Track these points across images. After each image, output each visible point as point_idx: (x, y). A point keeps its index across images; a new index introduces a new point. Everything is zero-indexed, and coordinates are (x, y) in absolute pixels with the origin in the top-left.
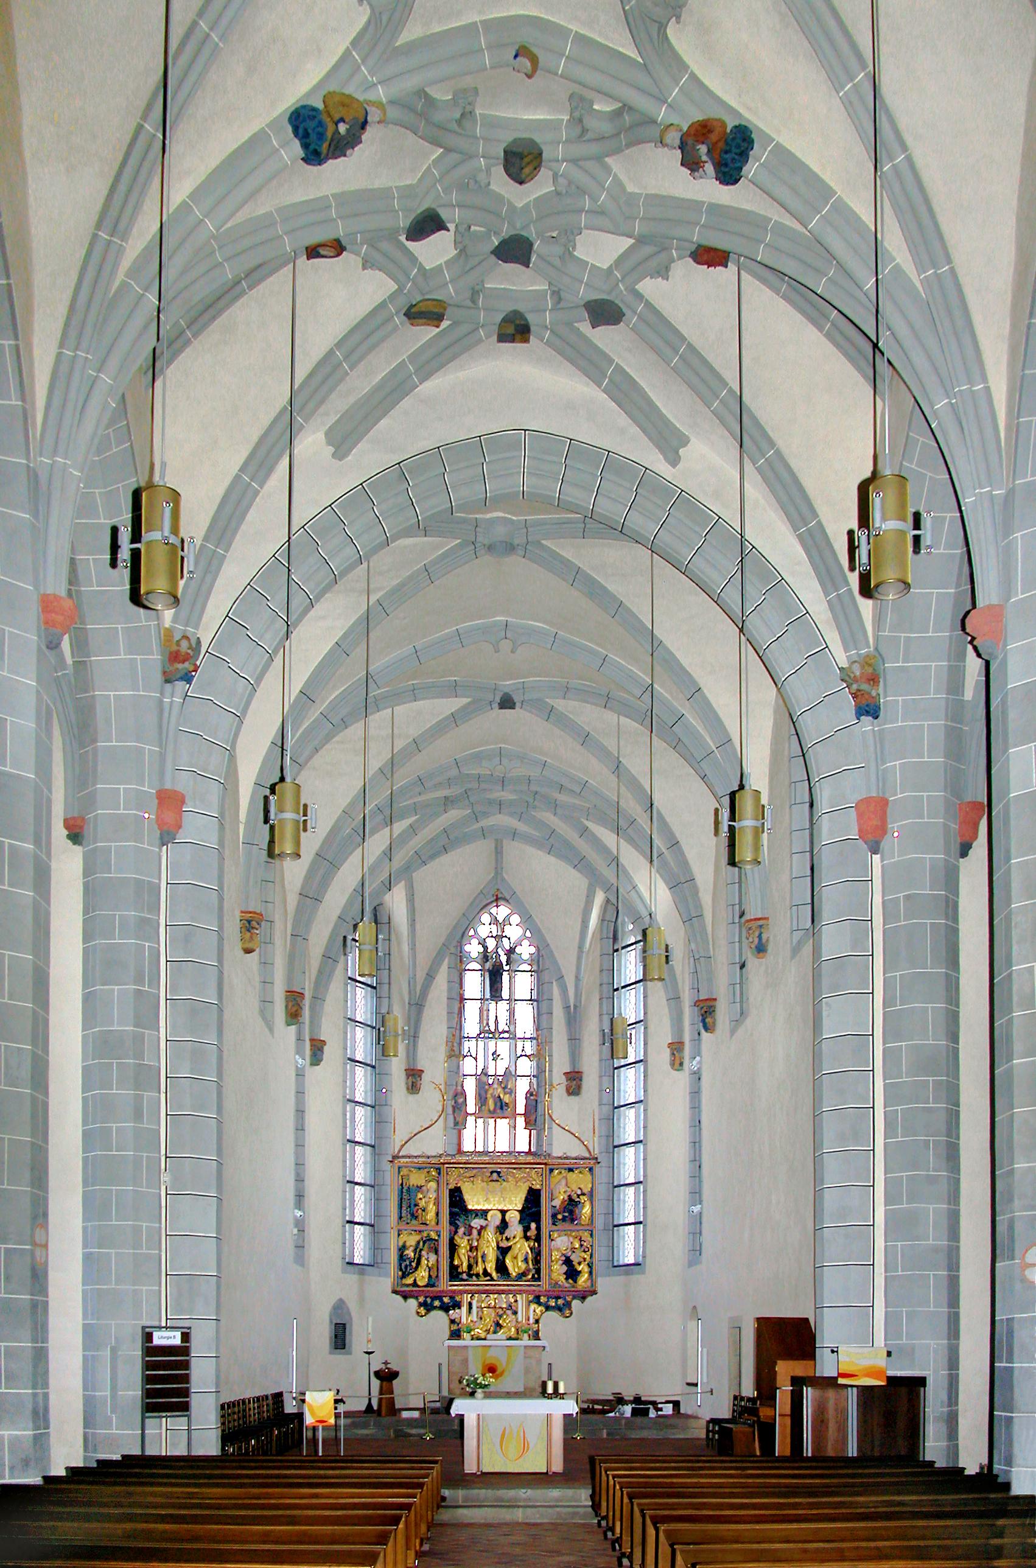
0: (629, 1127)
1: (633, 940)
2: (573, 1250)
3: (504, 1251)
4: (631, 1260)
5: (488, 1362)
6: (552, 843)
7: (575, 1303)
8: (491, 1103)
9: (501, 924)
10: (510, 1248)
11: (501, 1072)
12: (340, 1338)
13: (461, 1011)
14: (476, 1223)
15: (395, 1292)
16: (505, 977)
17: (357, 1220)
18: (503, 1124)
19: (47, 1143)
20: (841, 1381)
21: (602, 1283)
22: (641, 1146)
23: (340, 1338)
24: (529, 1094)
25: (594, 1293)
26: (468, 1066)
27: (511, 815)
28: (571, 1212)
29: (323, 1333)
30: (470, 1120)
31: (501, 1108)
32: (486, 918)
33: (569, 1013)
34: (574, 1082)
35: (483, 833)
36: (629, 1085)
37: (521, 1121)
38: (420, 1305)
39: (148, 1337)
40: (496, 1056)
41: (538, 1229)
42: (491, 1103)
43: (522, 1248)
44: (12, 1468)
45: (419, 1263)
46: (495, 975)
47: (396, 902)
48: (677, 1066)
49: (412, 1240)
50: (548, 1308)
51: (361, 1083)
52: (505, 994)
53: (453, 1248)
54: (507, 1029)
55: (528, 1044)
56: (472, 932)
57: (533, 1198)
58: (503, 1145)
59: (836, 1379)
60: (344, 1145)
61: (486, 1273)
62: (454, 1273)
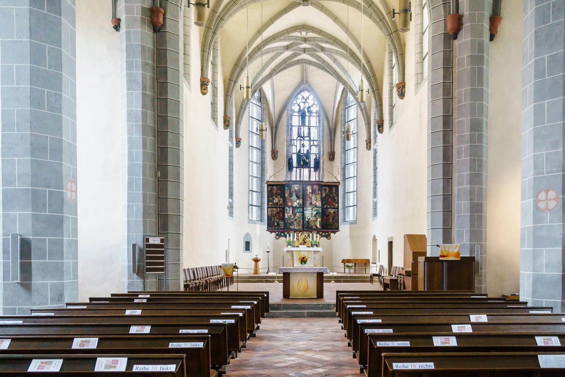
0: (351, 171)
1: (353, 104)
6: (324, 67)
7: (332, 235)
8: (302, 162)
9: (306, 100)
11: (305, 152)
12: (248, 246)
13: (291, 130)
16: (307, 118)
17: (254, 204)
18: (306, 171)
19: (76, 143)
20: (440, 259)
23: (248, 246)
24: (316, 159)
26: (294, 150)
27: (309, 54)
29: (242, 245)
30: (294, 169)
32: (300, 97)
34: (332, 156)
35: (298, 62)
36: (351, 156)
37: (312, 170)
38: (277, 235)
39: (147, 240)
40: (303, 146)
42: (302, 162)
44: (52, 299)
46: (303, 115)
47: (267, 88)
50: (322, 236)
51: (255, 155)
52: (307, 124)
55: (315, 142)
56: (295, 102)
58: (306, 179)
59: (439, 258)
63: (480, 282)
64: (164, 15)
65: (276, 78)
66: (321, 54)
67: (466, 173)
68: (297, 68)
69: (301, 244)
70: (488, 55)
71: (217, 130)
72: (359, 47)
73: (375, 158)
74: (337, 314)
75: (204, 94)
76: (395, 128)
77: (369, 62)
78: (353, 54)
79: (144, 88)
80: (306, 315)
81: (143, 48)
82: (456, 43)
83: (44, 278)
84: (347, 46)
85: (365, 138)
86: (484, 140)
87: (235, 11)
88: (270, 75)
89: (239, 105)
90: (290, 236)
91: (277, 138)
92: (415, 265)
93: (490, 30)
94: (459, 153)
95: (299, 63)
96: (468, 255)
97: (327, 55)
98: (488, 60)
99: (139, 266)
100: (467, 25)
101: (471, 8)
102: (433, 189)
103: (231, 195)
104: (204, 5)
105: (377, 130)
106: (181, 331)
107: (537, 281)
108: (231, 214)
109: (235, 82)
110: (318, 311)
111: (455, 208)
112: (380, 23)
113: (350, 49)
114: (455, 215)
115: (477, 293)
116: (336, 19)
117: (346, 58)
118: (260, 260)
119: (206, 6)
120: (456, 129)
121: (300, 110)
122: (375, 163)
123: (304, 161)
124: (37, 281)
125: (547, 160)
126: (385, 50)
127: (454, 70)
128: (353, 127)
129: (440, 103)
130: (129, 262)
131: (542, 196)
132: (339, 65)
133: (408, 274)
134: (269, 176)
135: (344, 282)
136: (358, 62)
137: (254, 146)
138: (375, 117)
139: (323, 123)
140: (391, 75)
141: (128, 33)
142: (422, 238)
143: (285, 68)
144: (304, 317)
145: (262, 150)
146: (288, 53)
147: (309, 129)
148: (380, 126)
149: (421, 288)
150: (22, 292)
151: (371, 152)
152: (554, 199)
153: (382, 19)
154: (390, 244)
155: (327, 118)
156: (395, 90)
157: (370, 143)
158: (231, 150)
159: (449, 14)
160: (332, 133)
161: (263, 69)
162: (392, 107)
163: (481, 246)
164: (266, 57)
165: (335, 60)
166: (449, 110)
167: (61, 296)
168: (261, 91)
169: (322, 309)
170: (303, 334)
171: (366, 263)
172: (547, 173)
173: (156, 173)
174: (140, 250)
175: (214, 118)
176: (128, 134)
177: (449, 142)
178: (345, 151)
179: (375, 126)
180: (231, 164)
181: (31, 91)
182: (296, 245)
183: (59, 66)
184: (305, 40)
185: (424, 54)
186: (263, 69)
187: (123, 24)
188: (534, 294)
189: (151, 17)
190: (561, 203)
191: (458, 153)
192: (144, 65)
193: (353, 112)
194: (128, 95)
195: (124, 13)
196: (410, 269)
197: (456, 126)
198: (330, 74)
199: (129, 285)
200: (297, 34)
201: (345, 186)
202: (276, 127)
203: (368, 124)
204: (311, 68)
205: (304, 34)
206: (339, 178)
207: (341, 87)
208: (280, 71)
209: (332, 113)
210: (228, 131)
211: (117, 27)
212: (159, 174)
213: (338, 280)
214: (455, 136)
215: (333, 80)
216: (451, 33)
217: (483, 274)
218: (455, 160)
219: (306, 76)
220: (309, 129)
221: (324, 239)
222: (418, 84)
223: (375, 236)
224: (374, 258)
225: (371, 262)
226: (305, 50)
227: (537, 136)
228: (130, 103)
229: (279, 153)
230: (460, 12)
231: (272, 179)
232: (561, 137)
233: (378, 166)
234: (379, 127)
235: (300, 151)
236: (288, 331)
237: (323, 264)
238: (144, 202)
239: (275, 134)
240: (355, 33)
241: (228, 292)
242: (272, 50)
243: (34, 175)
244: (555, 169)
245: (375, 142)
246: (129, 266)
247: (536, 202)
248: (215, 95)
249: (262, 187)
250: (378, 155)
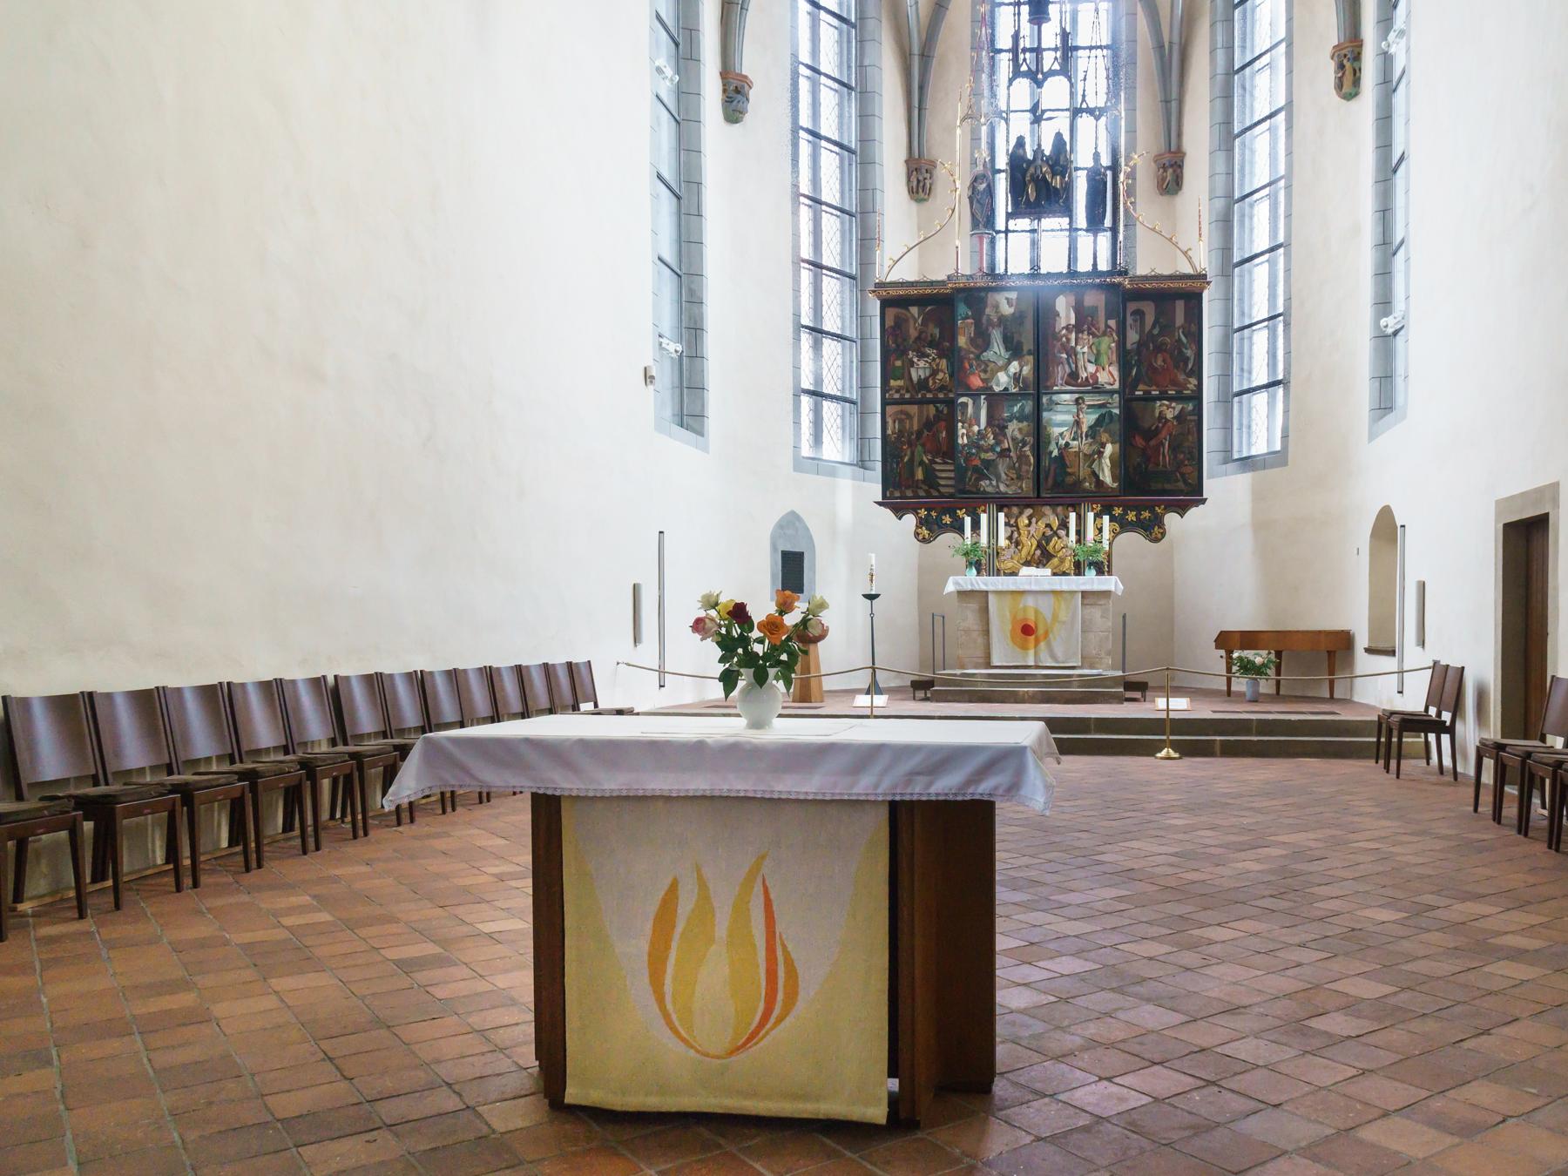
0: (1258, 230)
4: (1259, 448)
5: (1020, 616)
18: (1053, 223)
22: (1280, 391)
31: (1048, 199)
33: (1162, 57)
38: (921, 523)
48: (1347, 88)
54: (1056, 67)
60: (796, 396)
69: (1027, 563)
90: (976, 526)
91: (929, 104)
123: (1042, 184)
135: (1231, 751)
145: (859, 156)
157: (1357, 57)
160: (1172, 65)
178: (1228, 136)
202: (926, 56)
206: (1203, 258)
223: (1386, 516)
231: (906, 272)
233: (1409, 220)
235: (1020, 142)
239: (921, 88)
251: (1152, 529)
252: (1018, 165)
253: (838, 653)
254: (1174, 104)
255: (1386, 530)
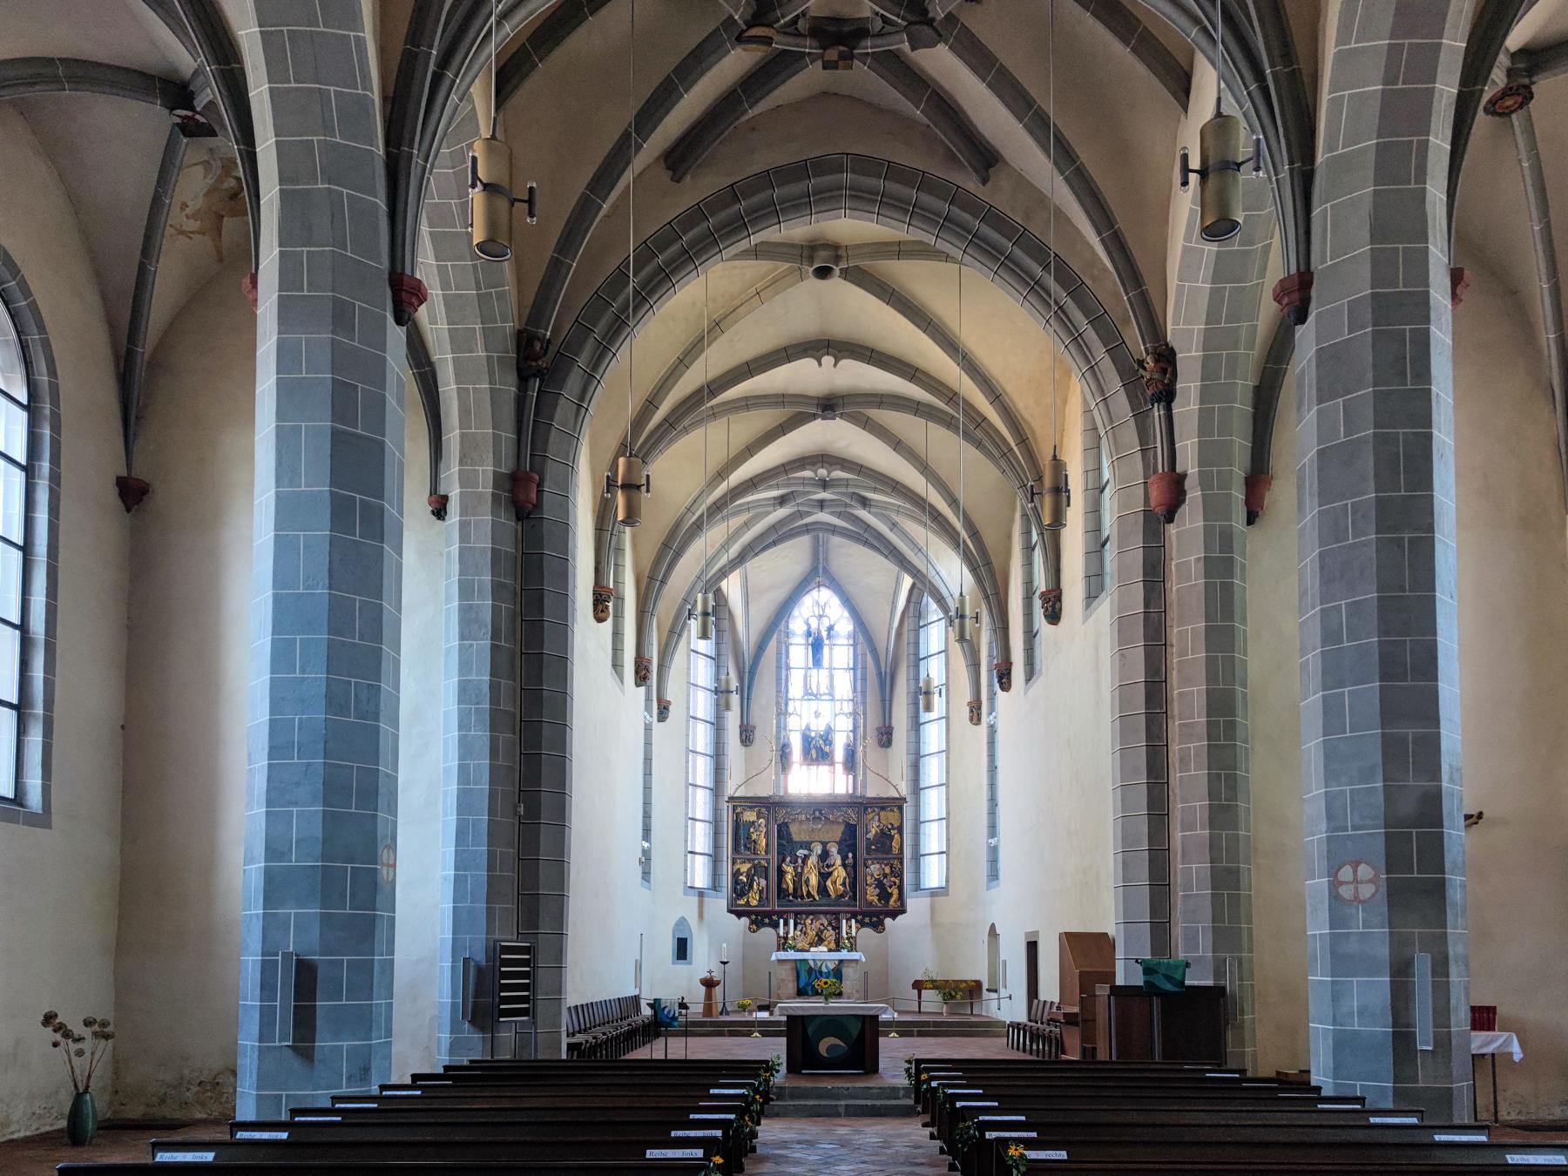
2: (885, 876)
3: (824, 876)
8: (813, 752)
10: (830, 874)
12: (682, 949)
14: (801, 852)
15: (730, 911)
16: (826, 650)
21: (910, 903)
23: (682, 949)
25: (904, 912)
27: (832, 513)
28: (883, 844)
29: (669, 947)
34: (885, 737)
35: (807, 529)
36: (933, 737)
37: (839, 768)
38: (752, 922)
40: (817, 714)
41: (854, 857)
42: (813, 752)
43: (840, 873)
44: (349, 1078)
45: (751, 886)
46: (816, 646)
47: (732, 587)
49: (745, 868)
53: (781, 873)
57: (851, 831)
61: (809, 894)
62: (782, 892)
63: (1241, 1042)
64: (540, 485)
65: (752, 565)
66: (862, 513)
67: (1201, 804)
68: (804, 541)
69: (811, 945)
70: (1243, 555)
71: (623, 691)
72: (953, 502)
73: (992, 743)
74: (919, 1109)
75: (600, 620)
76: (1038, 683)
77: (975, 534)
78: (937, 517)
79: (495, 635)
80: (842, 1110)
81: (495, 553)
82: (1172, 530)
83: (336, 1036)
84: (925, 501)
85: (968, 697)
86: (1239, 733)
87: (672, 441)
88: (741, 559)
89: (667, 627)
90: (786, 924)
91: (753, 696)
92: (1087, 1000)
93: (1247, 503)
94: (1184, 761)
95: (808, 531)
96: (1210, 983)
97: (875, 515)
98: (1243, 567)
99: (475, 1003)
100: (1194, 493)
101: (1202, 462)
102: (1126, 838)
103: (647, 833)
104: (639, 487)
105: (997, 686)
106: (673, 1134)
107: (1343, 1043)
108: (646, 874)
109: (663, 582)
110: (869, 1103)
111: (1178, 879)
112: (1002, 462)
113: (931, 506)
114: (1179, 894)
115: (1234, 1067)
116: (897, 444)
117: (921, 522)
118: (718, 983)
119: (644, 489)
120: (1175, 708)
121: (809, 634)
122: (992, 756)
124: (323, 1043)
125: (1352, 801)
126: (1014, 511)
127: (1168, 586)
128: (934, 670)
129: (1140, 654)
130: (454, 996)
131: (1346, 873)
132: (905, 535)
133: (1071, 1020)
134: (732, 787)
135: (920, 1034)
136: (946, 531)
137: (699, 716)
138: (990, 656)
139: (864, 662)
140: (1028, 564)
141: (464, 525)
142: (1101, 943)
143: (774, 543)
144: (839, 1115)
145: (718, 726)
146: (782, 512)
147: (831, 677)
148: (1004, 677)
149: (1102, 1055)
150: (295, 1063)
151: (983, 730)
152: (1370, 881)
153: (1006, 453)
154: (1032, 947)
155: (874, 651)
156: (1037, 603)
157: (980, 708)
158: (648, 729)
159: (1155, 471)
161: (725, 546)
162: (1030, 635)
163: (1240, 964)
164: (736, 522)
165: (894, 526)
166: (1159, 669)
167: (365, 1073)
168: (718, 593)
169: (879, 1098)
170: (843, 1151)
171: (973, 990)
172: (1354, 828)
173: (515, 807)
174: (479, 970)
175: (617, 665)
176: (461, 728)
177: (1159, 738)
178: (916, 725)
179: (990, 671)
180: (648, 760)
181: (328, 685)
182: (799, 946)
183: (378, 637)
184: (824, 484)
185: (1106, 533)
186: (725, 546)
187: (454, 507)
188: (1337, 1071)
189: (511, 491)
190: (1383, 890)
191: (1181, 760)
192: (497, 588)
193: (935, 636)
194: (462, 650)
195: (457, 485)
196: (1076, 1010)
197: (1176, 704)
198: (881, 553)
199: (454, 1048)
200: (808, 473)
201: (917, 806)
202: (752, 673)
203: (975, 666)
204: (836, 540)
205: (822, 472)
206: (904, 789)
207: (908, 581)
208: (764, 549)
209: (885, 637)
210: (642, 689)
211: (440, 512)
212: (522, 810)
213: (905, 1029)
214: (1175, 726)
215: (887, 566)
216: (1160, 511)
217: (1247, 1024)
218: (1176, 776)
219: (826, 559)
220: (831, 677)
221: (867, 931)
222: (1091, 597)
223: (993, 926)
224: (993, 976)
225: (985, 986)
226: (821, 504)
227: (1331, 754)
228: (464, 666)
229: (758, 733)
230: (1178, 470)
232: (1378, 758)
233: (1001, 762)
234: (1000, 678)
236: (811, 1144)
237: (866, 991)
238: (491, 867)
240: (943, 473)
241: (666, 1061)
242: (748, 507)
243: (326, 840)
244: (1369, 822)
245: (992, 709)
246: (454, 1005)
247: (1335, 884)
248: (618, 616)
249: (716, 810)
250: (1001, 738)
251: (878, 926)
252: (807, 741)
253: (847, 986)
254: (774, 537)
255: (440, 512)
